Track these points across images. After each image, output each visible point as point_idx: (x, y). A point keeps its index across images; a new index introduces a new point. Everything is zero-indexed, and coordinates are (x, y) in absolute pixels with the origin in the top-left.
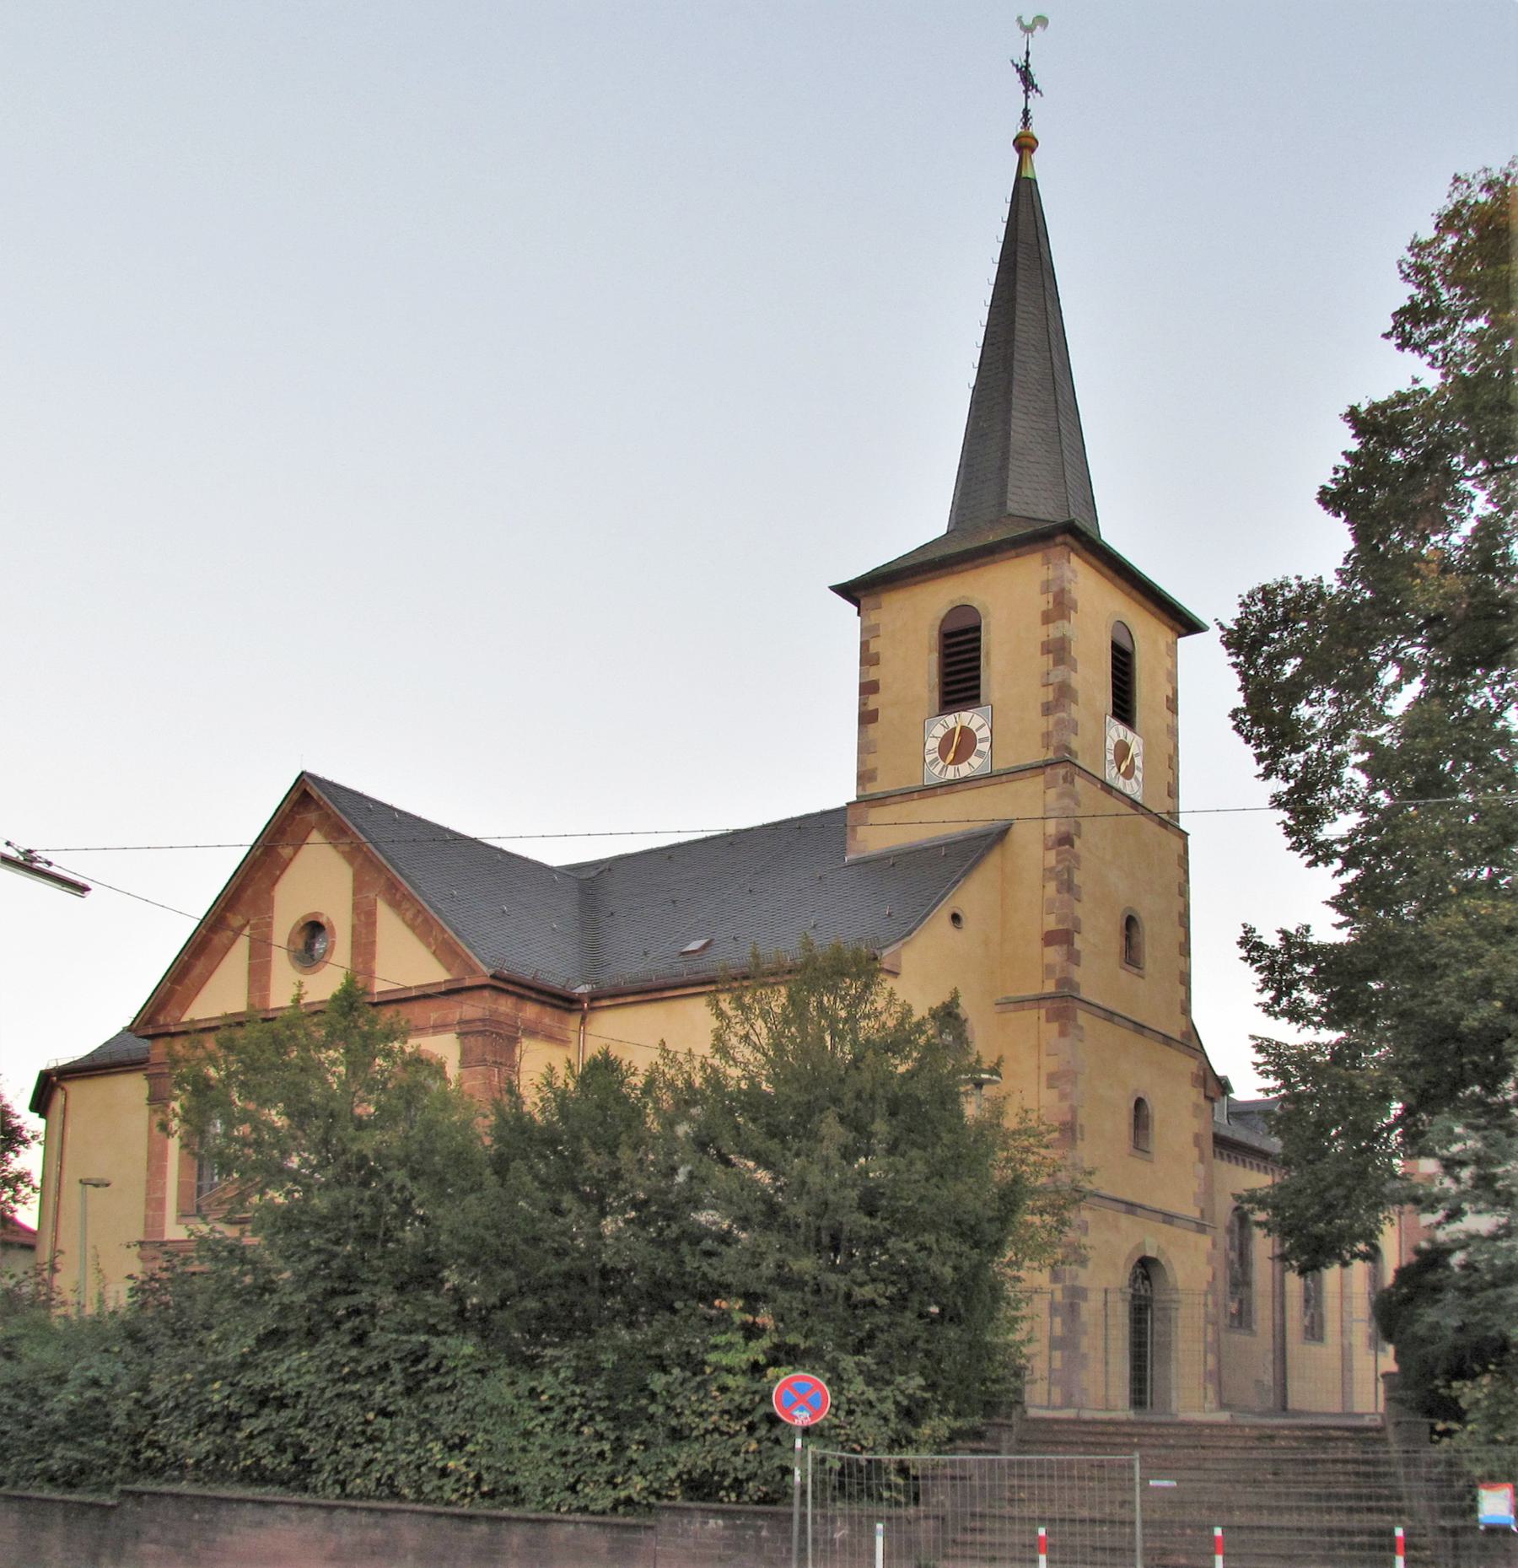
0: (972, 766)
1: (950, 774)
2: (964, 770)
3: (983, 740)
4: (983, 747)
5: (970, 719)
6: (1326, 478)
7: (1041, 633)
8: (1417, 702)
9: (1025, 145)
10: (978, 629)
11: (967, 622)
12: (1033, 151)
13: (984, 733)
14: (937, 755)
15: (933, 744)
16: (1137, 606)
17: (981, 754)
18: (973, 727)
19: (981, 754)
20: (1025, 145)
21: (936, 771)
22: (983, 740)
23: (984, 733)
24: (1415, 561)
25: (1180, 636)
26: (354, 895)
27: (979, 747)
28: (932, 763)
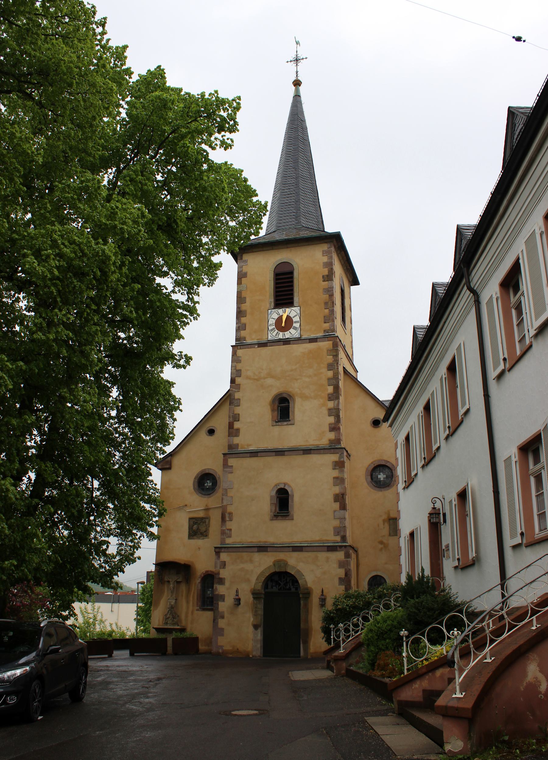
0: (292, 333)
1: (281, 336)
2: (287, 335)
3: (296, 322)
4: (297, 325)
5: (293, 312)
6: (128, 49)
7: (206, 287)
8: (320, 680)
9: (297, 83)
10: (292, 273)
11: (287, 270)
12: (300, 86)
13: (296, 319)
14: (274, 327)
15: (272, 321)
16: (341, 266)
17: (295, 328)
18: (292, 315)
19: (295, 328)
20: (297, 83)
21: (274, 334)
22: (296, 322)
23: (296, 319)
24: (155, 187)
25: (352, 285)
26: (236, 324)
27: (294, 325)
28: (272, 330)
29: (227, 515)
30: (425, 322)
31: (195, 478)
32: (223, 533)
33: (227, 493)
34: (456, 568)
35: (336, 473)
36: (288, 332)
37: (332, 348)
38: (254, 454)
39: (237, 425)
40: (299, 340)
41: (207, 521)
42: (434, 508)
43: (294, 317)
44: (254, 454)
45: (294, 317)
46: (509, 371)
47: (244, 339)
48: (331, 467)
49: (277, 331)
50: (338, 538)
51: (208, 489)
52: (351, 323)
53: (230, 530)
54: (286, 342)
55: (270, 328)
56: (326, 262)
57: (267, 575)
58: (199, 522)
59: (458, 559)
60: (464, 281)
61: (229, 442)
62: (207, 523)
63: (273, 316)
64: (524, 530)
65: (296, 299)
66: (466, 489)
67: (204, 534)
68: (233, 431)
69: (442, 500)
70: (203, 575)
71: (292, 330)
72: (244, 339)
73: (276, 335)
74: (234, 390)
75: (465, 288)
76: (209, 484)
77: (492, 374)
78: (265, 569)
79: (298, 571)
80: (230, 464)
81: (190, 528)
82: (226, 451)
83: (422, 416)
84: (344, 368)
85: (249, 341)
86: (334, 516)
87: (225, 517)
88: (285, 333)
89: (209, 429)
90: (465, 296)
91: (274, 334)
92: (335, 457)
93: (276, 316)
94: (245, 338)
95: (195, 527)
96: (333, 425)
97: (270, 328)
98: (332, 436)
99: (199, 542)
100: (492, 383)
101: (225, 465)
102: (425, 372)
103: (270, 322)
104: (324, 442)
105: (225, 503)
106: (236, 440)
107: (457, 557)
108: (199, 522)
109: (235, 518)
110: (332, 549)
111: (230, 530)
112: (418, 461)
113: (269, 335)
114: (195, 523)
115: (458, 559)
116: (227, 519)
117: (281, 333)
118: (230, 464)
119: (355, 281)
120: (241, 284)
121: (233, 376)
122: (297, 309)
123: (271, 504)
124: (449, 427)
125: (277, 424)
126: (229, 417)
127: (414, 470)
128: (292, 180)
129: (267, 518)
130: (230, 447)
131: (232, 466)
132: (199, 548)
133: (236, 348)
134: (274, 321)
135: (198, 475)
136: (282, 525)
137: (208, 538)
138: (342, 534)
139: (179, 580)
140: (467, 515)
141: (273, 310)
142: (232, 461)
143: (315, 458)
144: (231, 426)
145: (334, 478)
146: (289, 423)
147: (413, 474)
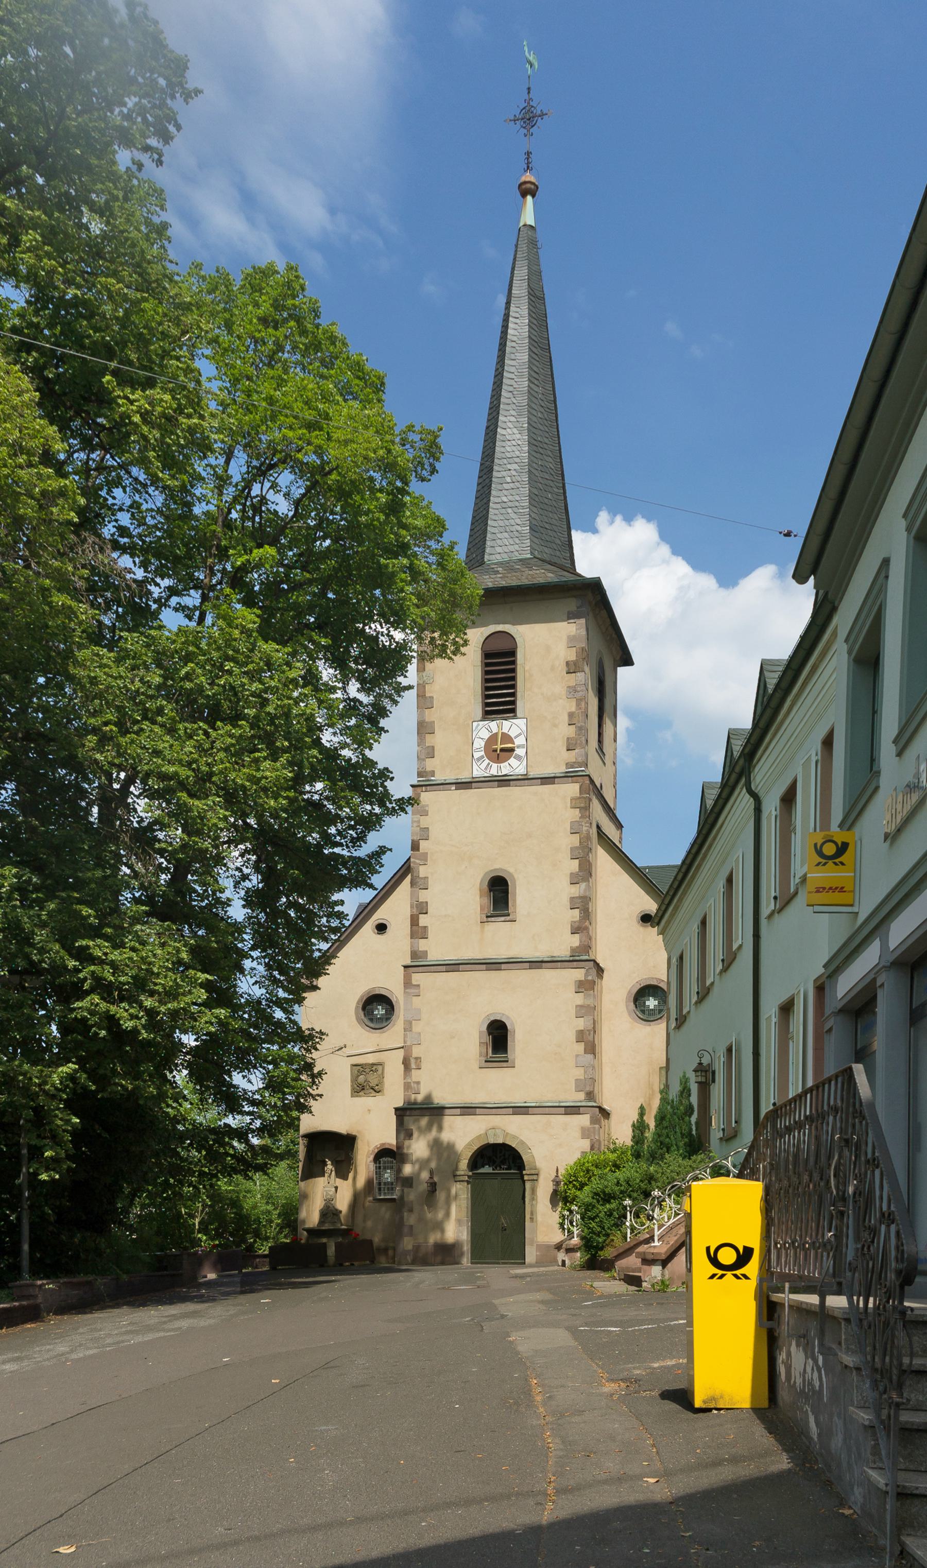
0: (513, 767)
4: (520, 752)
5: (513, 727)
9: (528, 154)
10: (512, 653)
14: (483, 753)
15: (479, 744)
19: (518, 758)
21: (483, 766)
28: (479, 759)
29: (413, 1061)
30: (745, 720)
31: (358, 1003)
32: (407, 1086)
33: (411, 1027)
34: (721, 1139)
35: (579, 999)
36: (506, 764)
37: (578, 795)
38: (453, 967)
39: (423, 920)
40: (525, 779)
41: (380, 1068)
42: (700, 1064)
43: (516, 737)
44: (453, 967)
45: (516, 737)
46: (778, 913)
47: (433, 773)
48: (573, 989)
49: (487, 761)
50: (582, 1096)
51: (380, 1020)
52: (615, 741)
53: (418, 1083)
54: (503, 781)
55: (476, 755)
56: (574, 636)
57: (476, 1148)
58: (367, 1070)
59: (723, 1130)
60: (743, 780)
61: (412, 946)
62: (380, 1072)
63: (481, 734)
64: (776, 1101)
65: (521, 706)
66: (793, 999)
67: (377, 1090)
68: (417, 931)
69: (712, 1054)
70: (376, 1151)
71: (512, 761)
72: (433, 773)
73: (486, 768)
74: (418, 861)
75: (744, 790)
76: (380, 1011)
77: (765, 911)
78: (472, 1141)
79: (522, 1143)
80: (414, 982)
81: (354, 1079)
82: (408, 962)
83: (776, 817)
84: (598, 827)
85: (439, 777)
86: (576, 1063)
87: (410, 1064)
88: (502, 765)
89: (377, 922)
90: (742, 803)
91: (482, 768)
92: (578, 974)
93: (486, 735)
94: (433, 772)
95: (361, 1079)
96: (577, 924)
97: (476, 755)
98: (576, 941)
99: (366, 1101)
100: (763, 922)
101: (408, 983)
102: (703, 874)
103: (476, 745)
104: (563, 952)
105: (408, 1043)
106: (422, 945)
107: (722, 1127)
108: (367, 1070)
109: (423, 1065)
110: (572, 1110)
111: (418, 1083)
112: (714, 965)
113: (475, 766)
114: (360, 1073)
115: (723, 1130)
116: (413, 1066)
117: (495, 765)
118: (414, 982)
119: (627, 660)
120: (424, 670)
121: (415, 838)
122: (521, 723)
123: (480, 1043)
124: (775, 898)
125: (489, 919)
126: (412, 907)
127: (709, 977)
128: (514, 448)
129: (476, 1065)
130: (415, 955)
131: (418, 986)
132: (369, 1110)
133: (419, 789)
134: (483, 744)
135: (362, 997)
136: (499, 927)
137: (383, 1095)
138: (588, 1089)
139: (339, 1159)
140: (792, 1038)
141: (481, 723)
142: (417, 978)
143: (547, 974)
144: (414, 921)
145: (577, 1006)
146: (508, 918)
147: (735, 947)
